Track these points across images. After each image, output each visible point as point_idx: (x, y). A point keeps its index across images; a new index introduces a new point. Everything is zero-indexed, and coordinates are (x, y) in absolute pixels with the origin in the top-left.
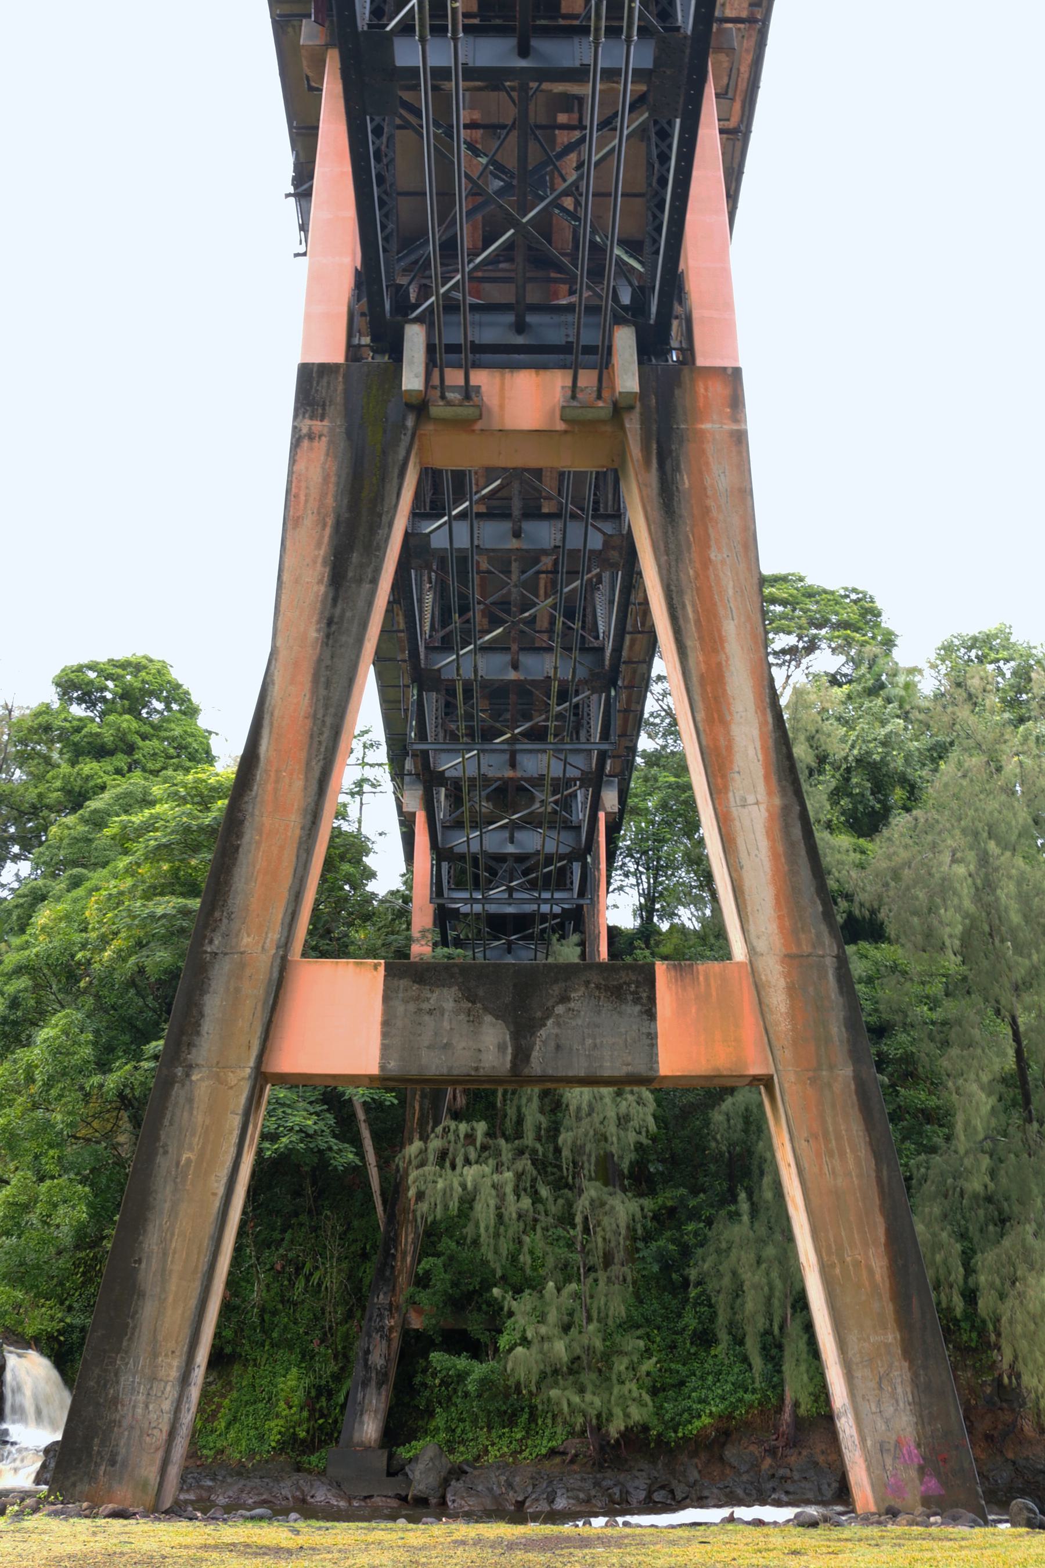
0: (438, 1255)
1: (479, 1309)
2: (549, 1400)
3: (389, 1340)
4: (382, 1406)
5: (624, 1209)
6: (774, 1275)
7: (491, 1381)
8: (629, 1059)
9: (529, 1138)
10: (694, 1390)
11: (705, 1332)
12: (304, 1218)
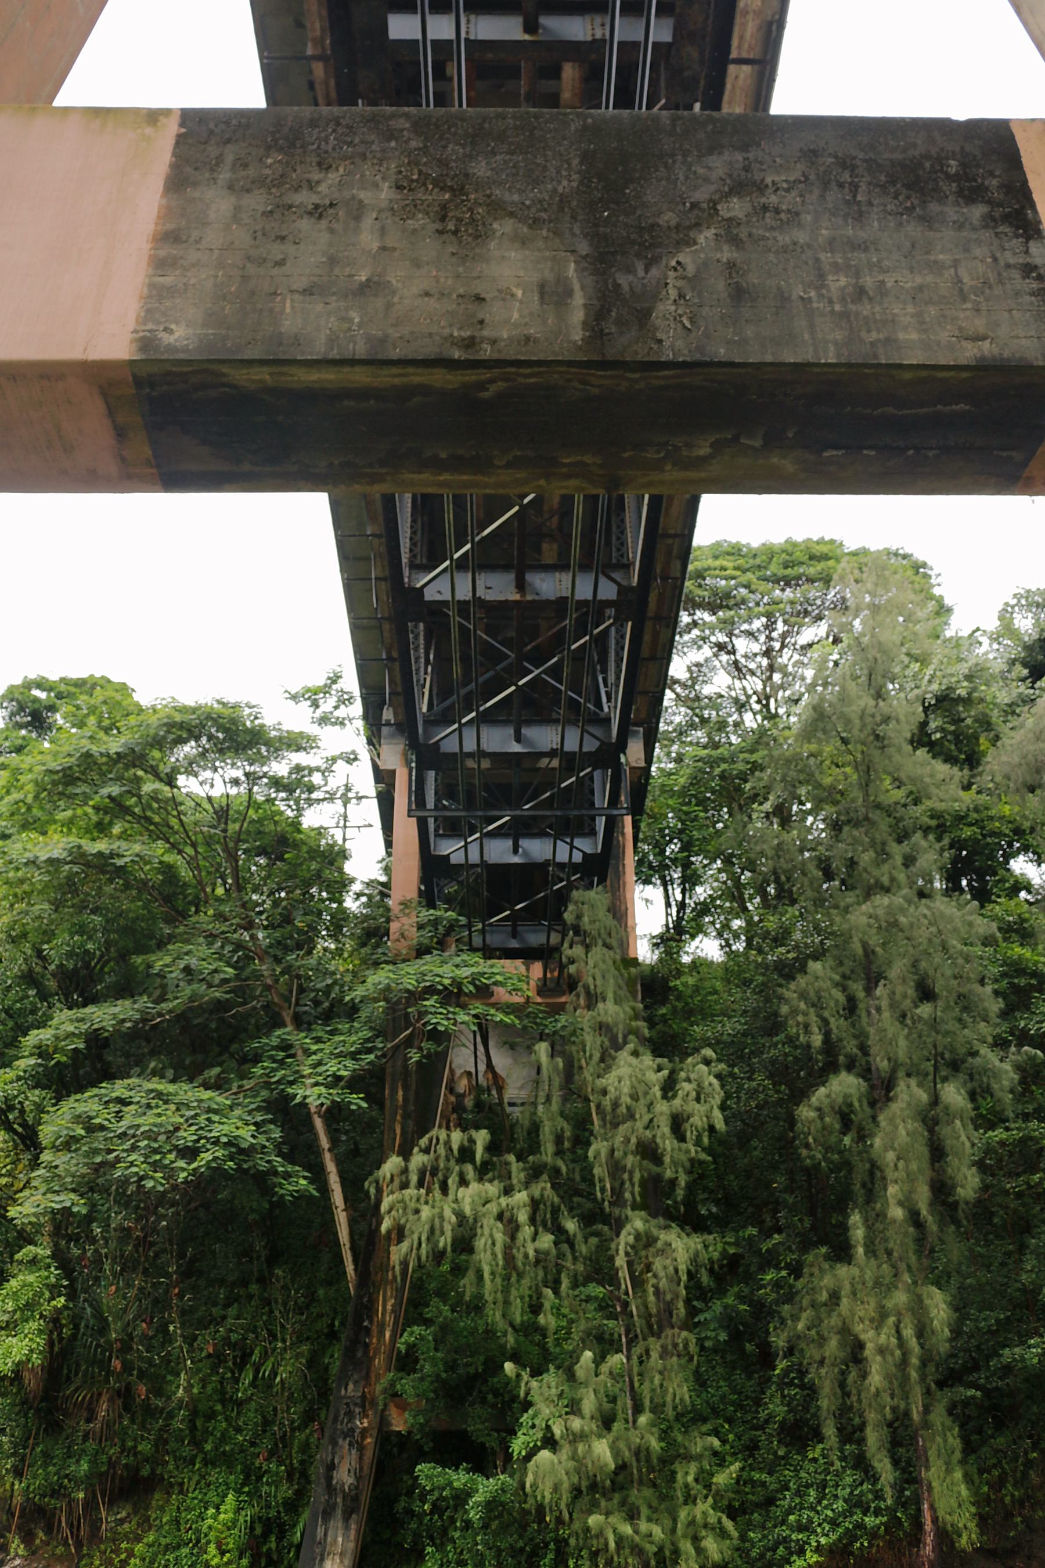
0: (427, 1323)
1: (483, 1401)
2: (588, 1530)
3: (361, 1449)
4: (351, 1545)
5: (681, 1248)
6: (908, 1332)
7: (503, 1504)
8: (980, 324)
9: (548, 1152)
10: (790, 1511)
11: (798, 1424)
12: (254, 1288)
